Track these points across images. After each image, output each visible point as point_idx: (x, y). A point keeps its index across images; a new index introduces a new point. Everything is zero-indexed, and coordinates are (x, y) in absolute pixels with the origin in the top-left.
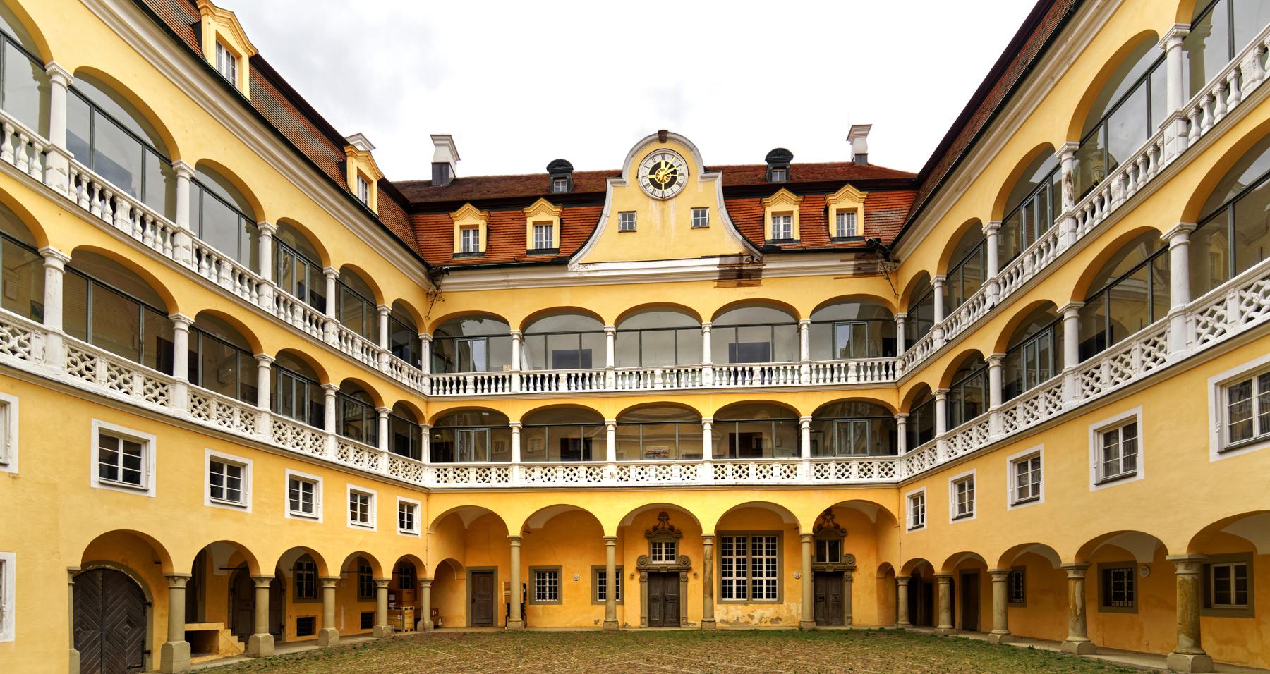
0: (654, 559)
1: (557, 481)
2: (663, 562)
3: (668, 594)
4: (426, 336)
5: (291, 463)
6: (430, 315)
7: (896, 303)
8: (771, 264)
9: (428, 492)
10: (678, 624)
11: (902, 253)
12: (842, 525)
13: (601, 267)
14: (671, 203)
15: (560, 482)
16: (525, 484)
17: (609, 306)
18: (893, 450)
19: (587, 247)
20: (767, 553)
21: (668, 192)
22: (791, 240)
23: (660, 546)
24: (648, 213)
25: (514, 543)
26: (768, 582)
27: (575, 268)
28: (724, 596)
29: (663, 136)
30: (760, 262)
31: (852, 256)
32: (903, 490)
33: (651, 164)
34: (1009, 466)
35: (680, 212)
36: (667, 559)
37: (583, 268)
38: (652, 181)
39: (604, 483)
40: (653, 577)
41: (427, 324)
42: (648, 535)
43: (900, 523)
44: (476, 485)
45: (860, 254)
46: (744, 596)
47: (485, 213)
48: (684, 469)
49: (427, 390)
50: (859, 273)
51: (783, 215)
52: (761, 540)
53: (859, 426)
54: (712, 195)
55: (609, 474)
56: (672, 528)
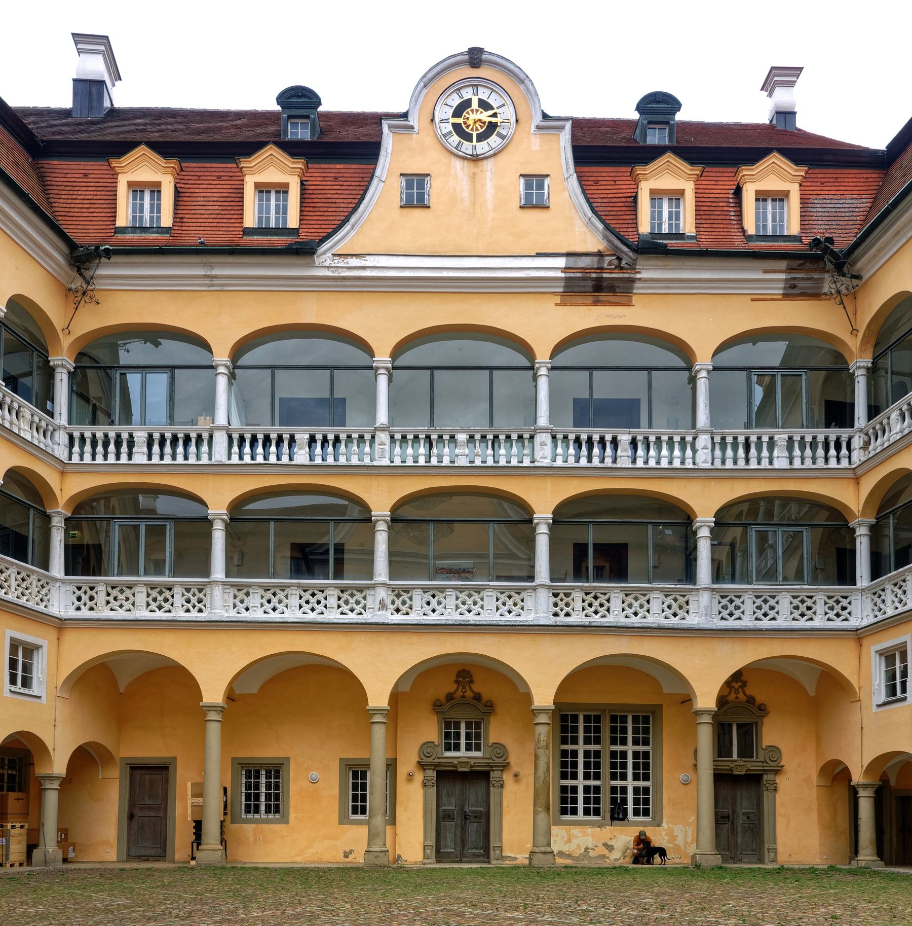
0: (448, 749)
1: (632, 615)
2: (462, 753)
6: (70, 328)
7: (853, 343)
8: (649, 271)
9: (61, 625)
11: (864, 263)
12: (760, 698)
14: (488, 165)
17: (382, 326)
18: (846, 575)
19: (347, 227)
21: (482, 147)
25: (213, 716)
27: (326, 261)
29: (475, 57)
30: (632, 267)
31: (783, 264)
33: (455, 101)
35: (501, 181)
36: (468, 748)
39: (368, 617)
40: (446, 777)
41: (66, 342)
42: (437, 707)
43: (862, 695)
44: (622, 621)
46: (597, 812)
47: (173, 163)
50: (792, 292)
51: (667, 194)
54: (557, 158)
56: (478, 697)
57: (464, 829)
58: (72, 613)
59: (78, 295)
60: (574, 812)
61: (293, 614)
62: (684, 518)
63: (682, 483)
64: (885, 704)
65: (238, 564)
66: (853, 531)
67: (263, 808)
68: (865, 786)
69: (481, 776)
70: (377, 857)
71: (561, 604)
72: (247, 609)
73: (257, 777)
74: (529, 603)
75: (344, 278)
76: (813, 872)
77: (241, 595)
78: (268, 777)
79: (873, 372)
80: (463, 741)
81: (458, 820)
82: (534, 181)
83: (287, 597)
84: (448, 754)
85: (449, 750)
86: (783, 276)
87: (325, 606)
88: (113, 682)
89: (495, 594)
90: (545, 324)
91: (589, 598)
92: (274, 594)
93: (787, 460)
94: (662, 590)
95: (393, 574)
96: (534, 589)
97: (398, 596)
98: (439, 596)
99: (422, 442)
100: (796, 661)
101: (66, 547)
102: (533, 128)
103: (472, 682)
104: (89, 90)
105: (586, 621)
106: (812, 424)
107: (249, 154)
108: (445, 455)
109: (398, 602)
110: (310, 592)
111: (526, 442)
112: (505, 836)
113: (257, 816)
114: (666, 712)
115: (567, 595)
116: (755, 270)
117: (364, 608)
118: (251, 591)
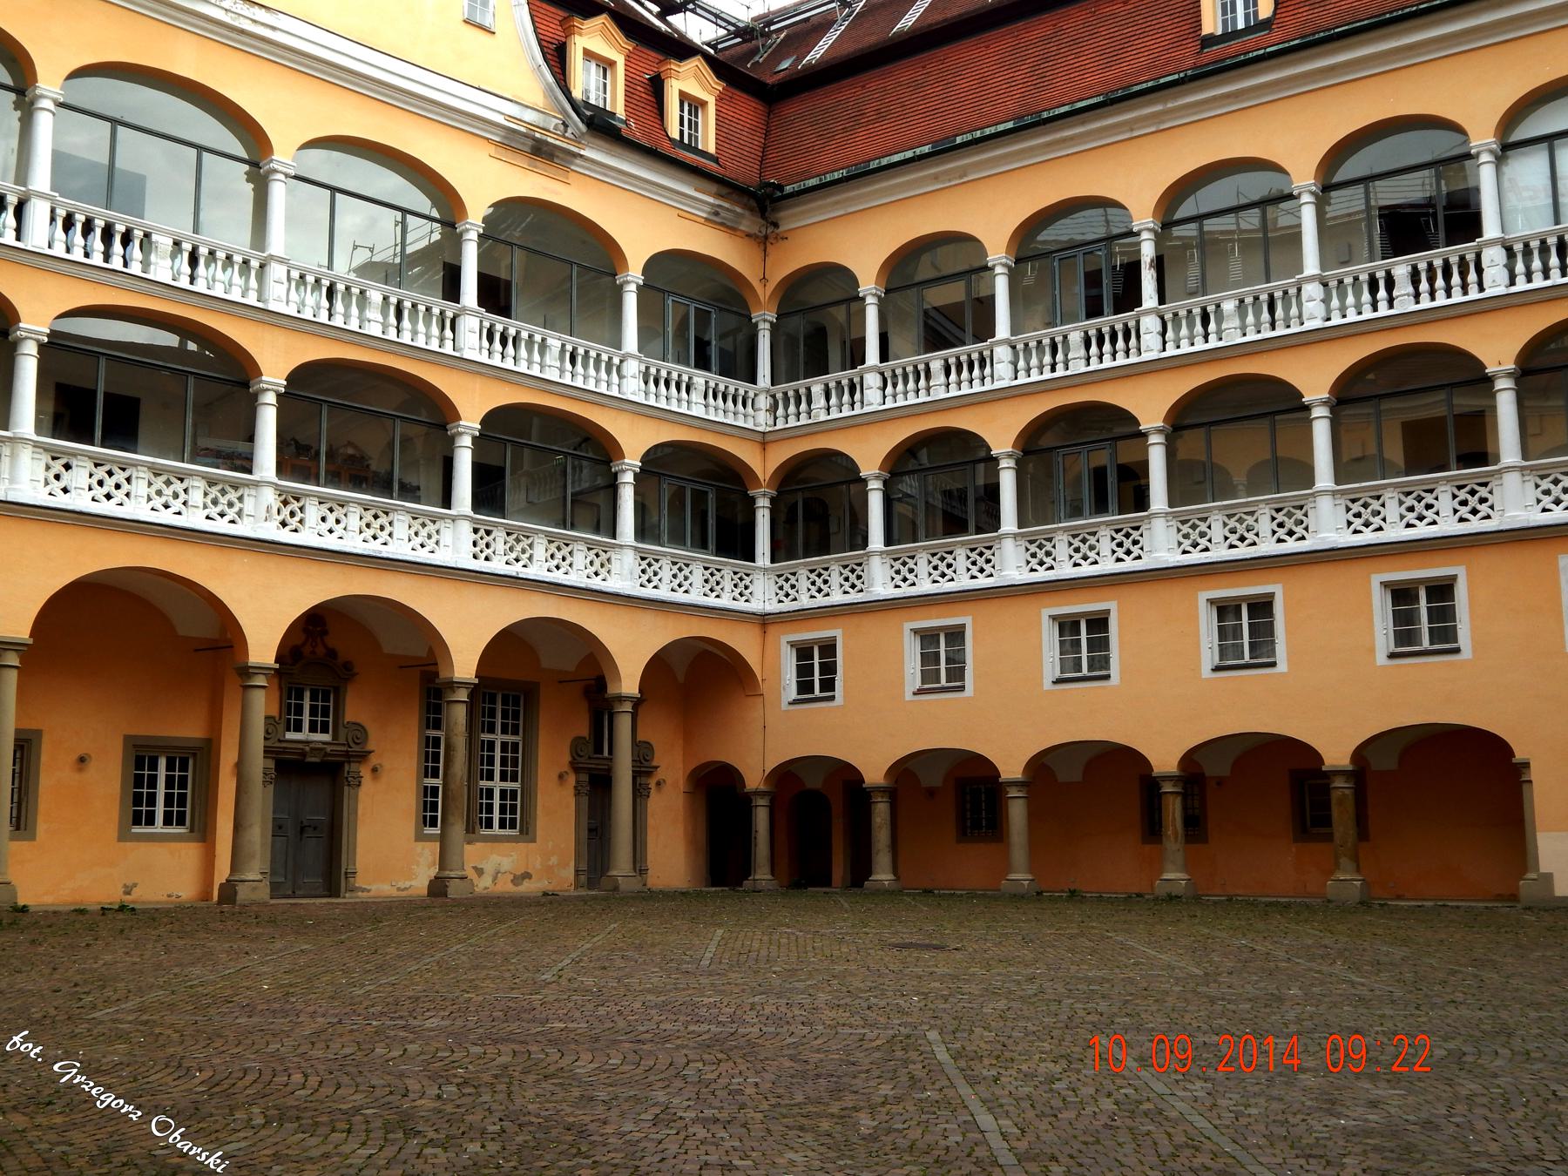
4: (764, 319)
5: (1045, 599)
6: (763, 275)
7: (764, 292)
10: (332, 889)
11: (792, 219)
16: (39, 496)
20: (504, 731)
22: (696, 151)
26: (503, 793)
28: (137, 821)
31: (714, 188)
32: (772, 630)
34: (1046, 624)
36: (313, 729)
40: (289, 767)
41: (764, 292)
45: (725, 191)
49: (750, 420)
53: (702, 500)
56: (332, 653)
58: (772, 607)
59: (765, 241)
60: (151, 821)
61: (137, 509)
63: (613, 413)
64: (795, 702)
65: (489, 495)
66: (753, 500)
71: (482, 544)
72: (65, 490)
73: (154, 766)
74: (447, 536)
75: (242, 32)
76: (684, 894)
77: (57, 467)
78: (170, 767)
80: (306, 718)
83: (128, 480)
84: (291, 735)
86: (711, 200)
87: (185, 503)
91: (368, 517)
92: (110, 473)
93: (699, 406)
95: (281, 469)
96: (454, 519)
97: (285, 503)
98: (339, 512)
99: (236, 267)
100: (166, 581)
101: (474, 463)
103: (326, 633)
105: (550, 577)
106: (423, 289)
108: (346, 317)
109: (286, 512)
110: (373, 512)
111: (253, 273)
112: (650, 858)
113: (149, 830)
116: (689, 184)
117: (240, 513)
118: (74, 463)
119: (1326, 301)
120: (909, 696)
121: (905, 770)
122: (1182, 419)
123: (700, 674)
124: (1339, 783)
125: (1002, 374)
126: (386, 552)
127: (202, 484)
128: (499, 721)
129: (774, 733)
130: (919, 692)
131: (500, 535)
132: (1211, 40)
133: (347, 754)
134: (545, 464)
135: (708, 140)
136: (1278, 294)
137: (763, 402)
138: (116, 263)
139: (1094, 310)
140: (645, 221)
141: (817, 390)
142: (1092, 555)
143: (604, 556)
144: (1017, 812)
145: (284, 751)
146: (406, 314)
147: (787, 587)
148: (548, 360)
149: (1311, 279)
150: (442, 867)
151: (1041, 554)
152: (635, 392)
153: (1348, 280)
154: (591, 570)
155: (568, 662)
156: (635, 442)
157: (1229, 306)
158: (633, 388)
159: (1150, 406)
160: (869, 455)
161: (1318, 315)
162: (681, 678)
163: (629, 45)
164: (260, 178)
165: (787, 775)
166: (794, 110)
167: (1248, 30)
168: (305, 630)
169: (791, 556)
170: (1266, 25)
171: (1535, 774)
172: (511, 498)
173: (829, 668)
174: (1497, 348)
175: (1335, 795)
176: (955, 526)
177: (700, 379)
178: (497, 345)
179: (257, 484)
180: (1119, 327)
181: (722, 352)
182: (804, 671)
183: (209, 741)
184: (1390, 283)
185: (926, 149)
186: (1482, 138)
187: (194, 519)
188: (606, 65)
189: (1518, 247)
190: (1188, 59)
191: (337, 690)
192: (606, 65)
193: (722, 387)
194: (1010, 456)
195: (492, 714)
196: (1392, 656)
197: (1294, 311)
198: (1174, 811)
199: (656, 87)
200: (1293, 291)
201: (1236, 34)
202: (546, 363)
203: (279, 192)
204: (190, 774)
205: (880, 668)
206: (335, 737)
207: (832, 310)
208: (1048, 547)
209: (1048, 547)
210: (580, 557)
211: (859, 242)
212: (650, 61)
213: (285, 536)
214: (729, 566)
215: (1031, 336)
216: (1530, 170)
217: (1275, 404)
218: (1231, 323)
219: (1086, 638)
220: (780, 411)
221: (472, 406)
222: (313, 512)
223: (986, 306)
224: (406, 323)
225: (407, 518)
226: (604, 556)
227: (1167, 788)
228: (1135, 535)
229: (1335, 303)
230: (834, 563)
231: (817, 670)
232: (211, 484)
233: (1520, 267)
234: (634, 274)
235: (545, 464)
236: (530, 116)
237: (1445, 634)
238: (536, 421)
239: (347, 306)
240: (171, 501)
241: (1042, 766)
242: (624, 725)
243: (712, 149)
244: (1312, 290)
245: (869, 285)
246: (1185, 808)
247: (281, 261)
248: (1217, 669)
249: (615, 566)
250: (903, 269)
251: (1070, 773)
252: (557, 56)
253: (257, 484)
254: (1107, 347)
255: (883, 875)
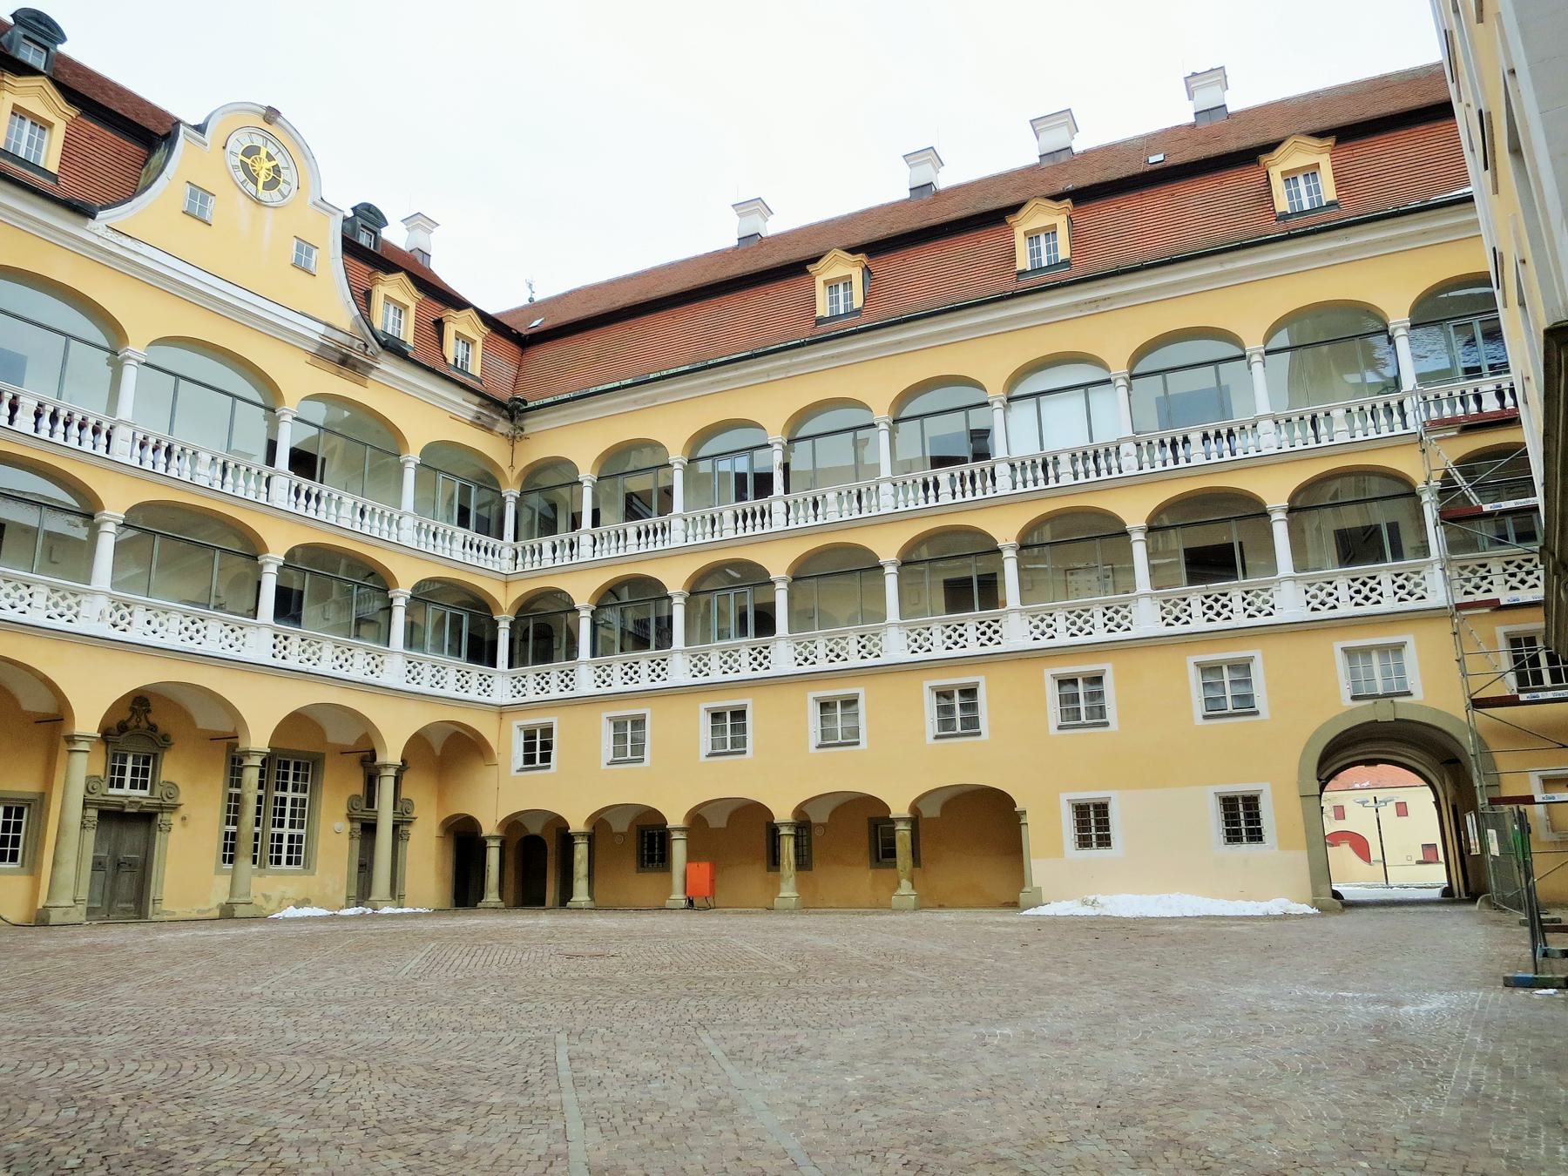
2: (126, 790)
3: (125, 855)
4: (511, 492)
8: (388, 365)
11: (532, 424)
13: (145, 250)
15: (173, 641)
19: (128, 206)
20: (295, 790)
23: (124, 760)
24: (229, 205)
29: (271, 115)
30: (374, 357)
31: (477, 400)
36: (133, 785)
37: (110, 235)
38: (244, 165)
40: (111, 817)
43: (499, 759)
48: (227, 630)
49: (503, 571)
50: (478, 423)
52: (287, 765)
53: (466, 625)
55: (93, 614)
56: (153, 728)
57: (115, 878)
58: (508, 700)
62: (252, 548)
64: (522, 770)
66: (497, 623)
67: (284, 860)
68: (495, 838)
69: (146, 819)
70: (65, 914)
71: (280, 647)
75: (111, 253)
79: (519, 502)
81: (109, 869)
82: (305, 248)
85: (111, 786)
88: (430, 748)
89: (180, 617)
90: (301, 380)
91: (187, 622)
94: (334, 641)
96: (258, 627)
97: (117, 609)
101: (278, 587)
102: (309, 202)
104: (531, 300)
107: (19, 74)
109: (117, 616)
113: (278, 867)
114: (328, 762)
115: (286, 638)
119: (895, 495)
120: (604, 766)
121: (599, 823)
122: (799, 575)
123: (452, 749)
124: (900, 826)
125: (677, 537)
126: (199, 649)
127: (46, 591)
128: (290, 782)
129: (499, 796)
130: (613, 763)
131: (295, 640)
132: (820, 321)
133: (160, 806)
134: (329, 586)
135: (475, 368)
136: (864, 490)
137: (508, 553)
138: (58, 438)
139: (741, 496)
140: (425, 416)
141: (547, 546)
142: (736, 666)
143: (378, 660)
144: (679, 850)
145: (106, 803)
146: (230, 471)
147: (519, 686)
148: (342, 512)
149: (885, 480)
150: (232, 894)
151: (700, 665)
152: (413, 542)
153: (910, 482)
154: (368, 669)
155: (349, 738)
156: (406, 577)
157: (831, 496)
158: (408, 536)
159: (778, 563)
160: (582, 591)
161: (889, 513)
162: (438, 752)
163: (421, 296)
164: (117, 365)
165: (513, 824)
166: (545, 355)
167: (846, 315)
168: (132, 709)
169: (524, 663)
170: (858, 312)
171: (1028, 819)
172: (308, 611)
173: (547, 746)
174: (1005, 530)
175: (898, 835)
176: (641, 643)
177: (460, 533)
178: (302, 499)
179: (93, 593)
180: (758, 509)
181: (478, 517)
182: (529, 747)
183: (43, 794)
184: (936, 485)
185: (629, 381)
186: (995, 390)
187: (37, 617)
188: (401, 308)
189: (1018, 464)
190: (807, 333)
191: (155, 755)
192: (401, 308)
193: (476, 541)
194: (680, 595)
195: (286, 776)
196: (937, 737)
197: (874, 501)
198: (788, 847)
199: (439, 325)
200: (873, 488)
201: (839, 317)
202: (340, 516)
203: (130, 374)
204: (24, 820)
205: (679, 736)
206: (152, 792)
207: (560, 490)
208: (706, 659)
209: (706, 659)
210: (360, 658)
211: (578, 441)
212: (435, 310)
213: (115, 634)
214: (476, 669)
215: (698, 513)
216: (1024, 413)
217: (867, 567)
218: (833, 507)
219: (731, 724)
220: (520, 560)
221: (278, 544)
222: (140, 616)
223: (668, 492)
224: (229, 478)
225: (220, 625)
226: (378, 660)
227: (784, 831)
228: (765, 652)
229: (901, 497)
230: (554, 669)
231: (538, 748)
232: (54, 591)
233: (1019, 478)
234: (413, 457)
235: (329, 586)
236: (339, 337)
237: (971, 724)
238: (343, 562)
239: (328, 507)
240: (17, 603)
241: (697, 819)
242: (386, 787)
243: (478, 374)
244: (886, 488)
245: (587, 474)
246: (796, 846)
247: (128, 424)
248: (820, 747)
249: (386, 667)
250: (615, 462)
251: (718, 821)
252: (364, 299)
253: (93, 593)
254: (749, 521)
255: (581, 893)
